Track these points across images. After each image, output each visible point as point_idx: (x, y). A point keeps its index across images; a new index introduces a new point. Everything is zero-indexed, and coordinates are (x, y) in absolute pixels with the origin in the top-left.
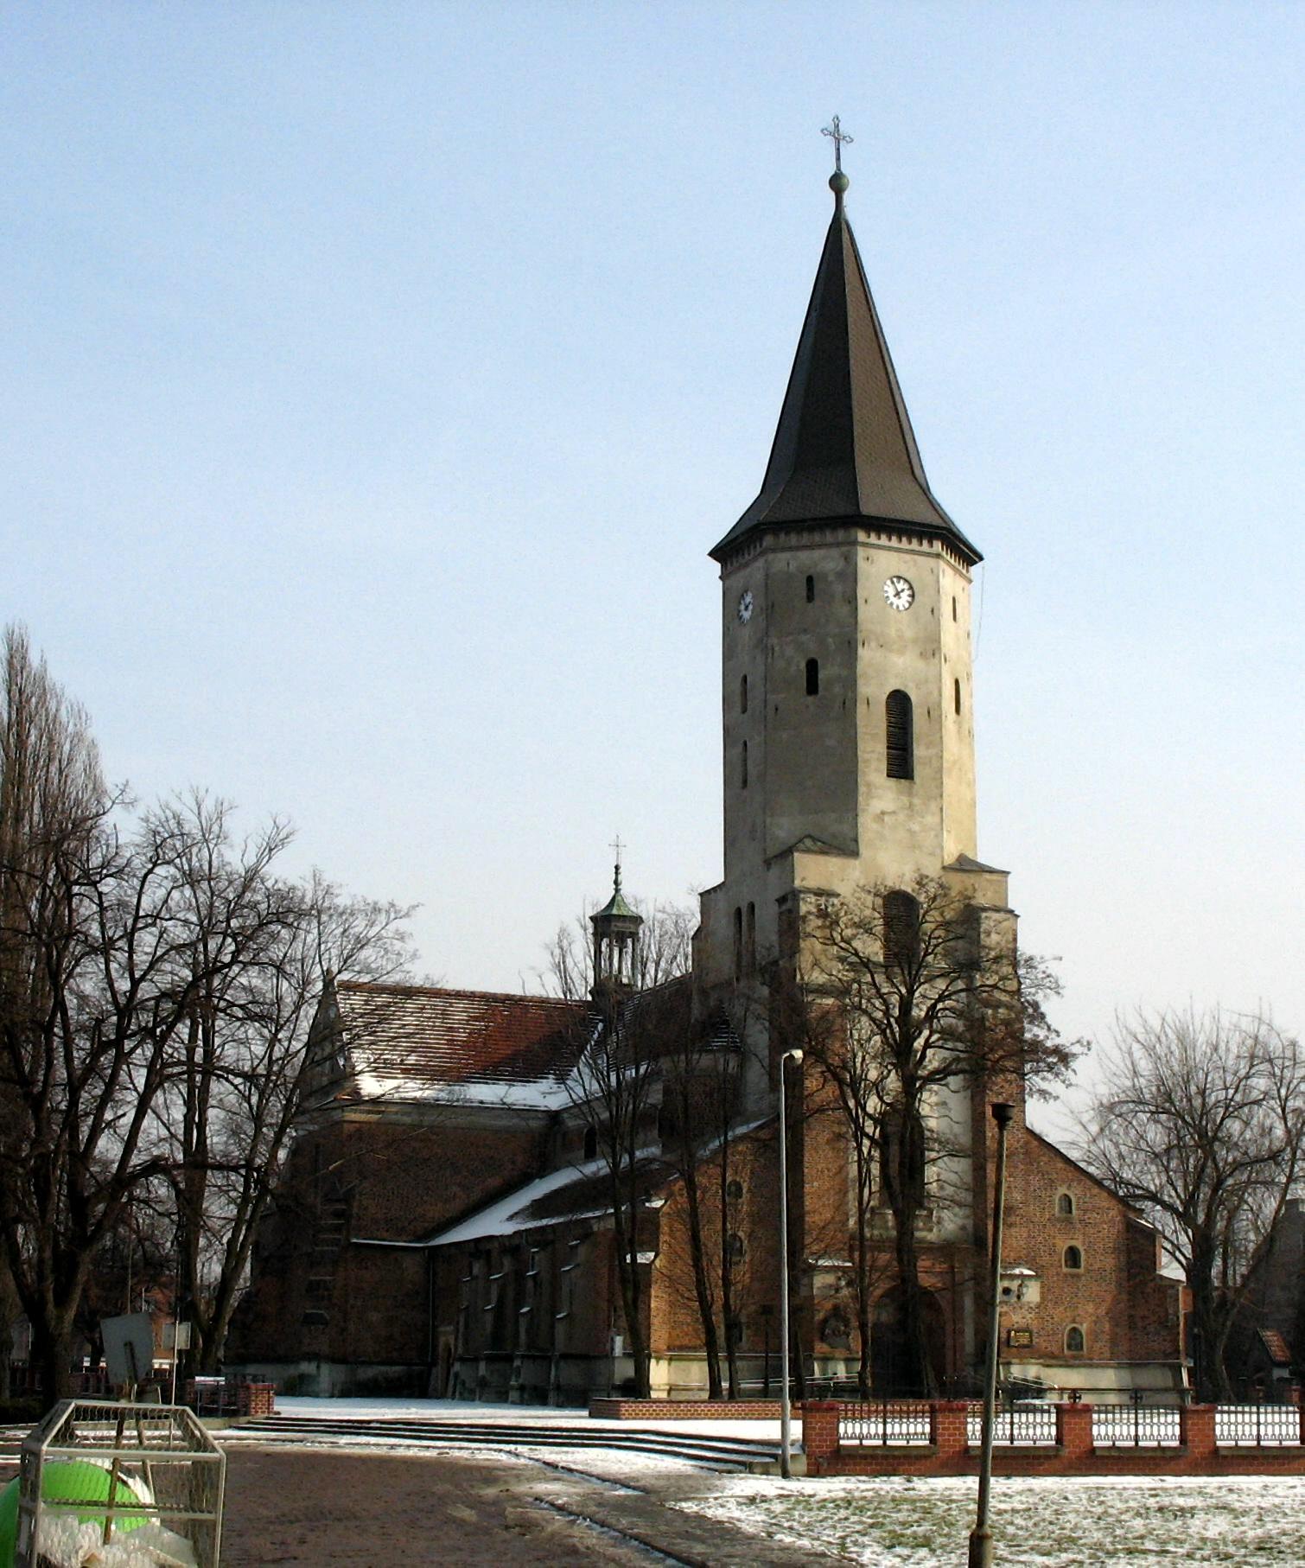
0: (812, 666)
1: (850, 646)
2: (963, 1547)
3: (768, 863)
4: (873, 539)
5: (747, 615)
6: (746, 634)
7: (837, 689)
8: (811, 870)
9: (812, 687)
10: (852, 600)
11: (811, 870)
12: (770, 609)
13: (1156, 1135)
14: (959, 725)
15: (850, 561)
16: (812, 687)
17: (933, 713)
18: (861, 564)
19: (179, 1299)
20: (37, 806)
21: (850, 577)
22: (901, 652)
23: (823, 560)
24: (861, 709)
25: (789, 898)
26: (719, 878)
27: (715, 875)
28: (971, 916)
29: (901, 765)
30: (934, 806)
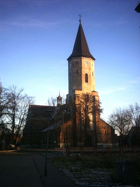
0: (77, 71)
1: (81, 69)
2: (54, 104)
3: (73, 92)
4: (83, 58)
5: (70, 66)
6: (70, 68)
7: (80, 73)
8: (77, 92)
9: (77, 74)
10: (81, 64)
11: (77, 92)
12: (72, 65)
13: (116, 119)
14: (93, 77)
15: (81, 60)
16: (77, 74)
17: (90, 76)
18: (82, 60)
19: (13, 126)
20: (94, 139)
21: (81, 62)
22: (87, 69)
23: (78, 60)
24: (82, 75)
25: (75, 95)
26: (68, 93)
27: (68, 93)
28: (94, 97)
29: (87, 81)
30: (90, 85)
